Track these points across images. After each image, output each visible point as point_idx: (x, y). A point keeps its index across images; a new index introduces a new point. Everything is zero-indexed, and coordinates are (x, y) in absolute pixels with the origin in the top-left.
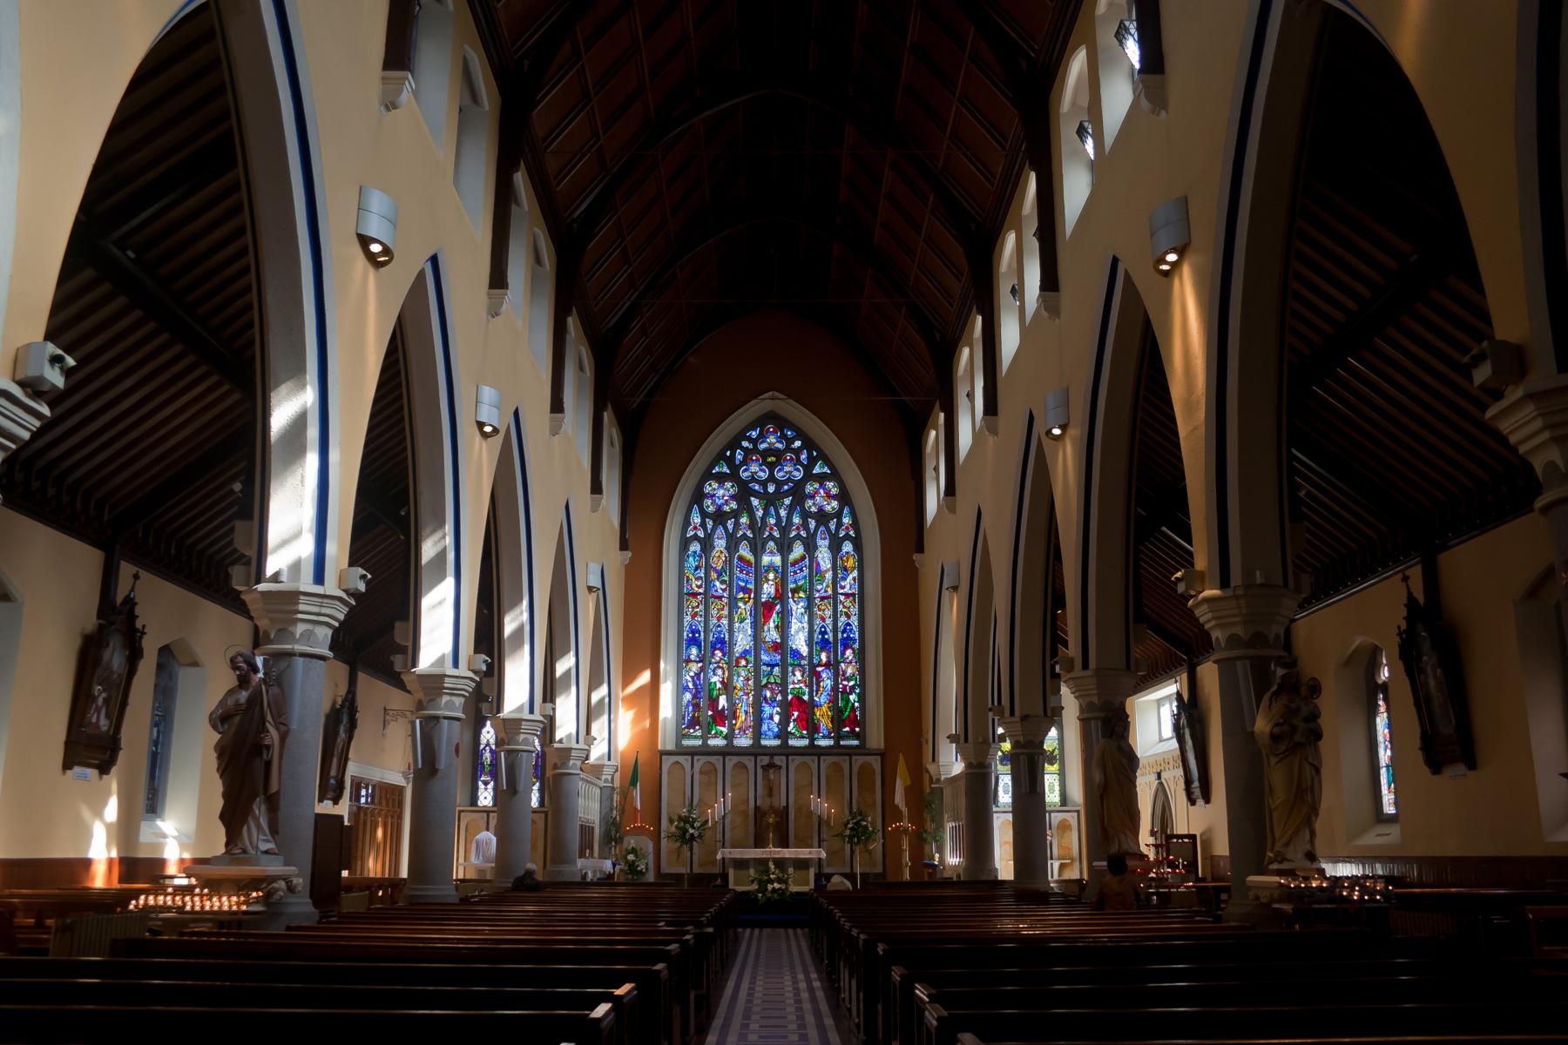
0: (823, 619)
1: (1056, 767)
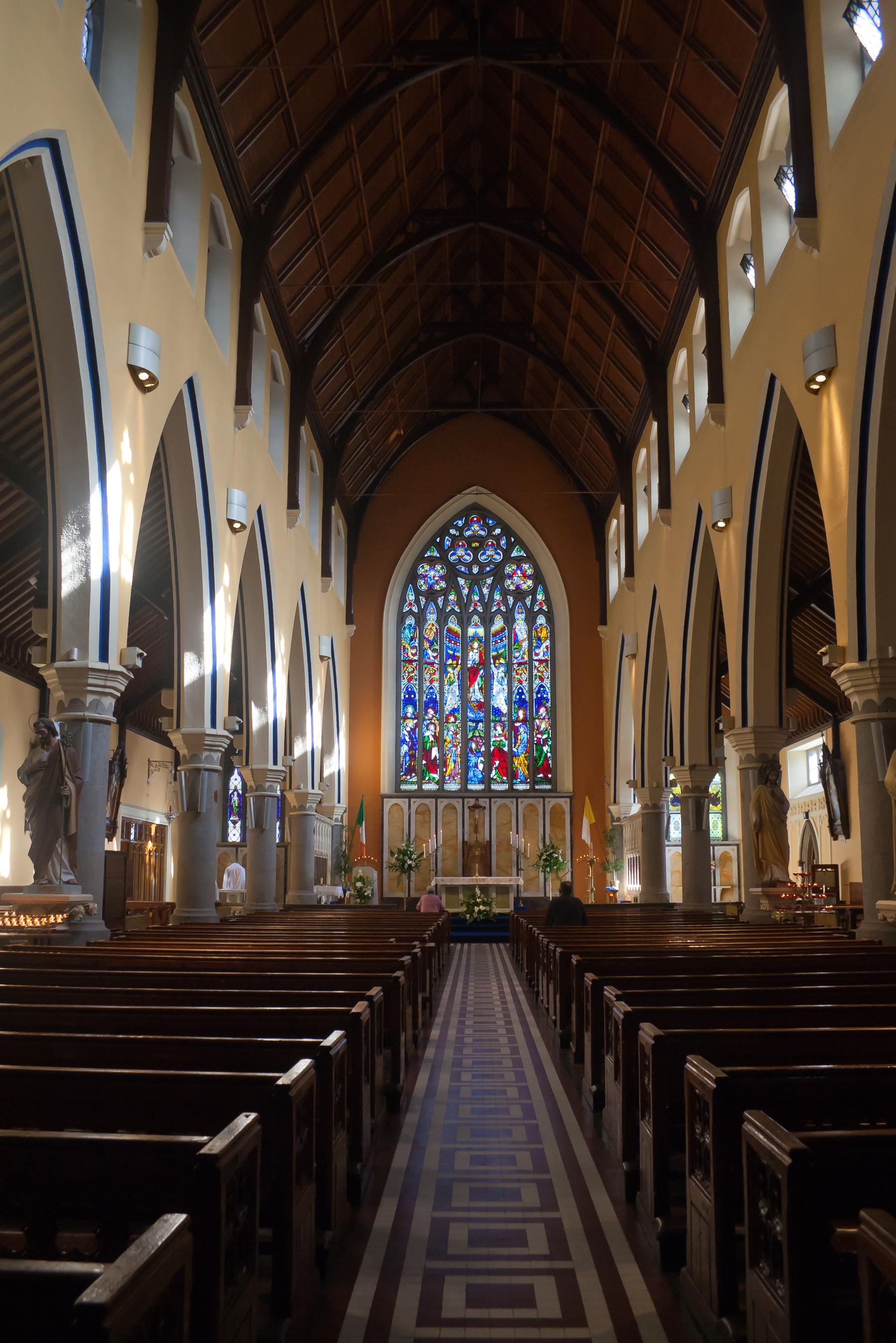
0: (520, 682)
1: (719, 808)
